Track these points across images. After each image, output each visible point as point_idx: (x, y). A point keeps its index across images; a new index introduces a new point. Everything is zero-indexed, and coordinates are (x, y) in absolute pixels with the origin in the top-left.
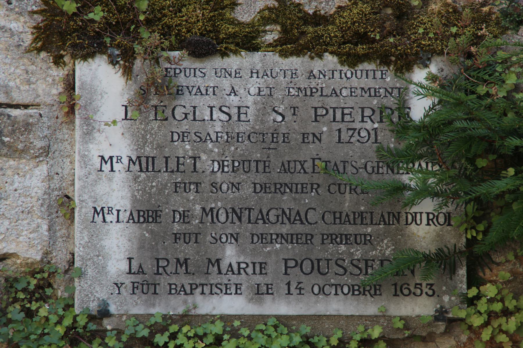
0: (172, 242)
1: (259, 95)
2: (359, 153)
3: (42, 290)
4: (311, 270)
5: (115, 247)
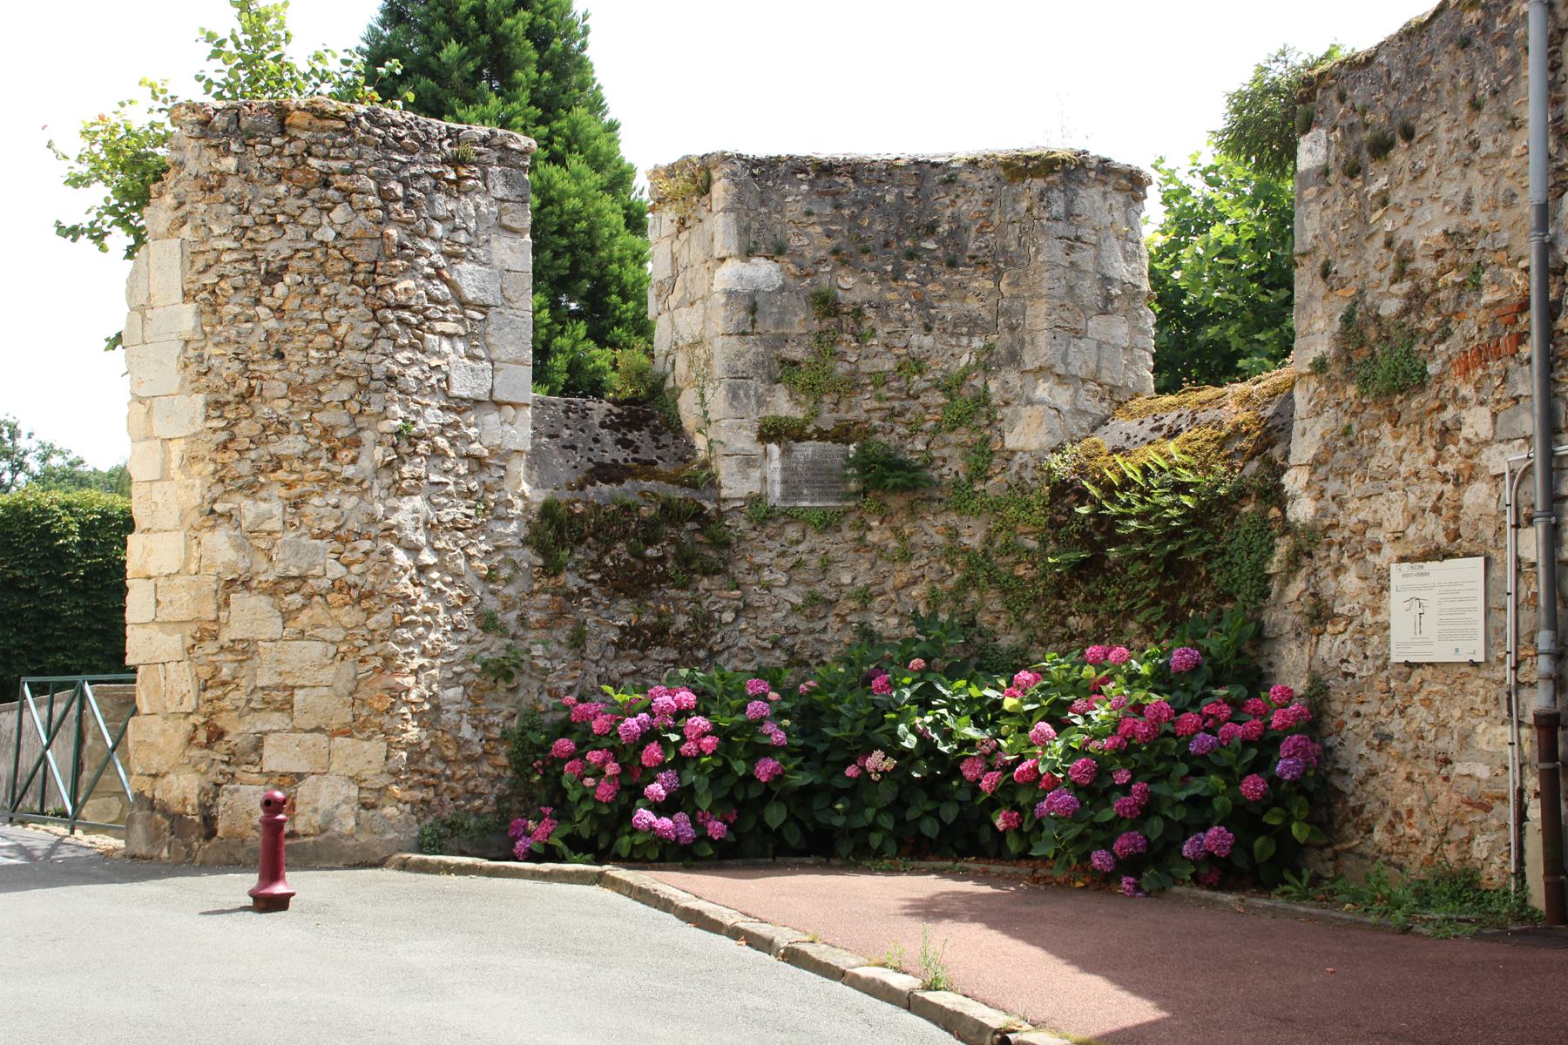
0: (791, 488)
1: (221, 173)
2: (837, 465)
3: (760, 500)
4: (825, 495)
5: (777, 490)
